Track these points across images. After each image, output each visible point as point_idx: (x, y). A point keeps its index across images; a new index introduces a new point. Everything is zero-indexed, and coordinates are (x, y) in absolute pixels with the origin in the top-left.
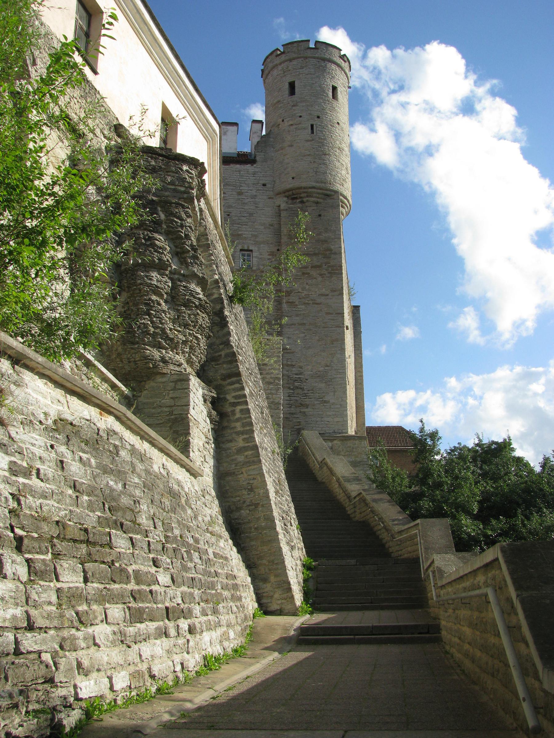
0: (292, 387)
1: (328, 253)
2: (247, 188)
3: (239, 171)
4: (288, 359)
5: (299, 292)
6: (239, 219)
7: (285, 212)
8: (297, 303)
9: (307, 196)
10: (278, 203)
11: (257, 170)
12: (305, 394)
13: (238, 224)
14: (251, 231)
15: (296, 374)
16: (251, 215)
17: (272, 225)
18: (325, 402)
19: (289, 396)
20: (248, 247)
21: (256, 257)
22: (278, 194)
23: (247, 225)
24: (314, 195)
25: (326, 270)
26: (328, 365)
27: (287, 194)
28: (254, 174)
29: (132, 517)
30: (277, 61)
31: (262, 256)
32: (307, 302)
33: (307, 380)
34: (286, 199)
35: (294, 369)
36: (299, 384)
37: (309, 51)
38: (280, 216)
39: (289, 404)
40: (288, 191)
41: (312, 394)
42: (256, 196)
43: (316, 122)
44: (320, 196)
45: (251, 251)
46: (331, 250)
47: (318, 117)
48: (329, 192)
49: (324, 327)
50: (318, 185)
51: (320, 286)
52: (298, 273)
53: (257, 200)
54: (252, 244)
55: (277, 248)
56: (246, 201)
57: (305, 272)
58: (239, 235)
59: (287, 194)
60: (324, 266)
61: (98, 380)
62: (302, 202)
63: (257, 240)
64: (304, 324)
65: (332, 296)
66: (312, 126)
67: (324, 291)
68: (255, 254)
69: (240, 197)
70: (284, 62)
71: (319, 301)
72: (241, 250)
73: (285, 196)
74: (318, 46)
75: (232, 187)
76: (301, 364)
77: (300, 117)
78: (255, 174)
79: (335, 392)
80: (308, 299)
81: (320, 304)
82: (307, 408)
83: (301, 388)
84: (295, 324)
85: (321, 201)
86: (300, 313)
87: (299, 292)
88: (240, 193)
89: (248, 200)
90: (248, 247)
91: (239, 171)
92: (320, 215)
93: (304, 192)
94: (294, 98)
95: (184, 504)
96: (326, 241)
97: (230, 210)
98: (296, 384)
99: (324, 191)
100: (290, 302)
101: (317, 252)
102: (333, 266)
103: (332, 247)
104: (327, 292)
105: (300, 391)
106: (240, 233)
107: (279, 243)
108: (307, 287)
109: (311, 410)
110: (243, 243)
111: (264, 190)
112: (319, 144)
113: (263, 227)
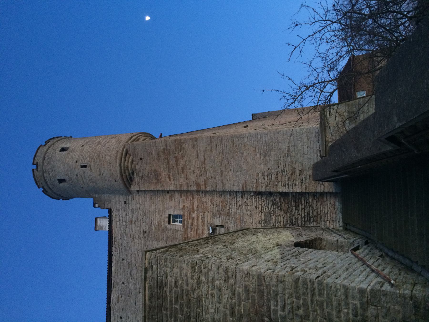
0: (276, 183)
1: (166, 152)
4: (251, 187)
5: (197, 176)
7: (141, 187)
9: (128, 170)
11: (115, 209)
12: (282, 170)
13: (151, 225)
15: (264, 179)
17: (151, 198)
18: (288, 151)
19: (285, 186)
20: (167, 217)
21: (174, 212)
24: (126, 163)
25: (178, 153)
26: (254, 149)
27: (128, 185)
28: (118, 210)
29: (334, 122)
31: (173, 206)
32: (203, 169)
33: (269, 169)
35: (260, 181)
36: (273, 176)
40: (125, 184)
41: (282, 163)
43: (80, 164)
44: (127, 159)
45: (170, 215)
46: (164, 149)
47: (77, 162)
48: (124, 153)
49: (223, 154)
51: (191, 158)
52: (183, 176)
54: (164, 214)
55: (166, 193)
56: (135, 217)
57: (181, 171)
58: (159, 225)
59: (128, 185)
60: (176, 155)
62: (133, 173)
64: (221, 171)
65: (197, 147)
66: (82, 167)
67: (194, 155)
68: (172, 213)
69: (133, 222)
71: (202, 159)
72: (169, 223)
73: (130, 187)
74: (35, 163)
76: (255, 174)
77: (77, 175)
79: (279, 142)
82: (295, 168)
83: (277, 174)
84: (222, 180)
86: (213, 176)
87: (197, 176)
88: (131, 222)
90: (167, 217)
92: (141, 159)
93: (125, 172)
96: (158, 154)
98: (273, 178)
100: (205, 184)
101: (166, 161)
102: (176, 148)
103: (162, 148)
104: (195, 152)
105: (280, 175)
107: (163, 191)
108: (192, 169)
109: (297, 164)
110: (164, 221)
112: (93, 161)
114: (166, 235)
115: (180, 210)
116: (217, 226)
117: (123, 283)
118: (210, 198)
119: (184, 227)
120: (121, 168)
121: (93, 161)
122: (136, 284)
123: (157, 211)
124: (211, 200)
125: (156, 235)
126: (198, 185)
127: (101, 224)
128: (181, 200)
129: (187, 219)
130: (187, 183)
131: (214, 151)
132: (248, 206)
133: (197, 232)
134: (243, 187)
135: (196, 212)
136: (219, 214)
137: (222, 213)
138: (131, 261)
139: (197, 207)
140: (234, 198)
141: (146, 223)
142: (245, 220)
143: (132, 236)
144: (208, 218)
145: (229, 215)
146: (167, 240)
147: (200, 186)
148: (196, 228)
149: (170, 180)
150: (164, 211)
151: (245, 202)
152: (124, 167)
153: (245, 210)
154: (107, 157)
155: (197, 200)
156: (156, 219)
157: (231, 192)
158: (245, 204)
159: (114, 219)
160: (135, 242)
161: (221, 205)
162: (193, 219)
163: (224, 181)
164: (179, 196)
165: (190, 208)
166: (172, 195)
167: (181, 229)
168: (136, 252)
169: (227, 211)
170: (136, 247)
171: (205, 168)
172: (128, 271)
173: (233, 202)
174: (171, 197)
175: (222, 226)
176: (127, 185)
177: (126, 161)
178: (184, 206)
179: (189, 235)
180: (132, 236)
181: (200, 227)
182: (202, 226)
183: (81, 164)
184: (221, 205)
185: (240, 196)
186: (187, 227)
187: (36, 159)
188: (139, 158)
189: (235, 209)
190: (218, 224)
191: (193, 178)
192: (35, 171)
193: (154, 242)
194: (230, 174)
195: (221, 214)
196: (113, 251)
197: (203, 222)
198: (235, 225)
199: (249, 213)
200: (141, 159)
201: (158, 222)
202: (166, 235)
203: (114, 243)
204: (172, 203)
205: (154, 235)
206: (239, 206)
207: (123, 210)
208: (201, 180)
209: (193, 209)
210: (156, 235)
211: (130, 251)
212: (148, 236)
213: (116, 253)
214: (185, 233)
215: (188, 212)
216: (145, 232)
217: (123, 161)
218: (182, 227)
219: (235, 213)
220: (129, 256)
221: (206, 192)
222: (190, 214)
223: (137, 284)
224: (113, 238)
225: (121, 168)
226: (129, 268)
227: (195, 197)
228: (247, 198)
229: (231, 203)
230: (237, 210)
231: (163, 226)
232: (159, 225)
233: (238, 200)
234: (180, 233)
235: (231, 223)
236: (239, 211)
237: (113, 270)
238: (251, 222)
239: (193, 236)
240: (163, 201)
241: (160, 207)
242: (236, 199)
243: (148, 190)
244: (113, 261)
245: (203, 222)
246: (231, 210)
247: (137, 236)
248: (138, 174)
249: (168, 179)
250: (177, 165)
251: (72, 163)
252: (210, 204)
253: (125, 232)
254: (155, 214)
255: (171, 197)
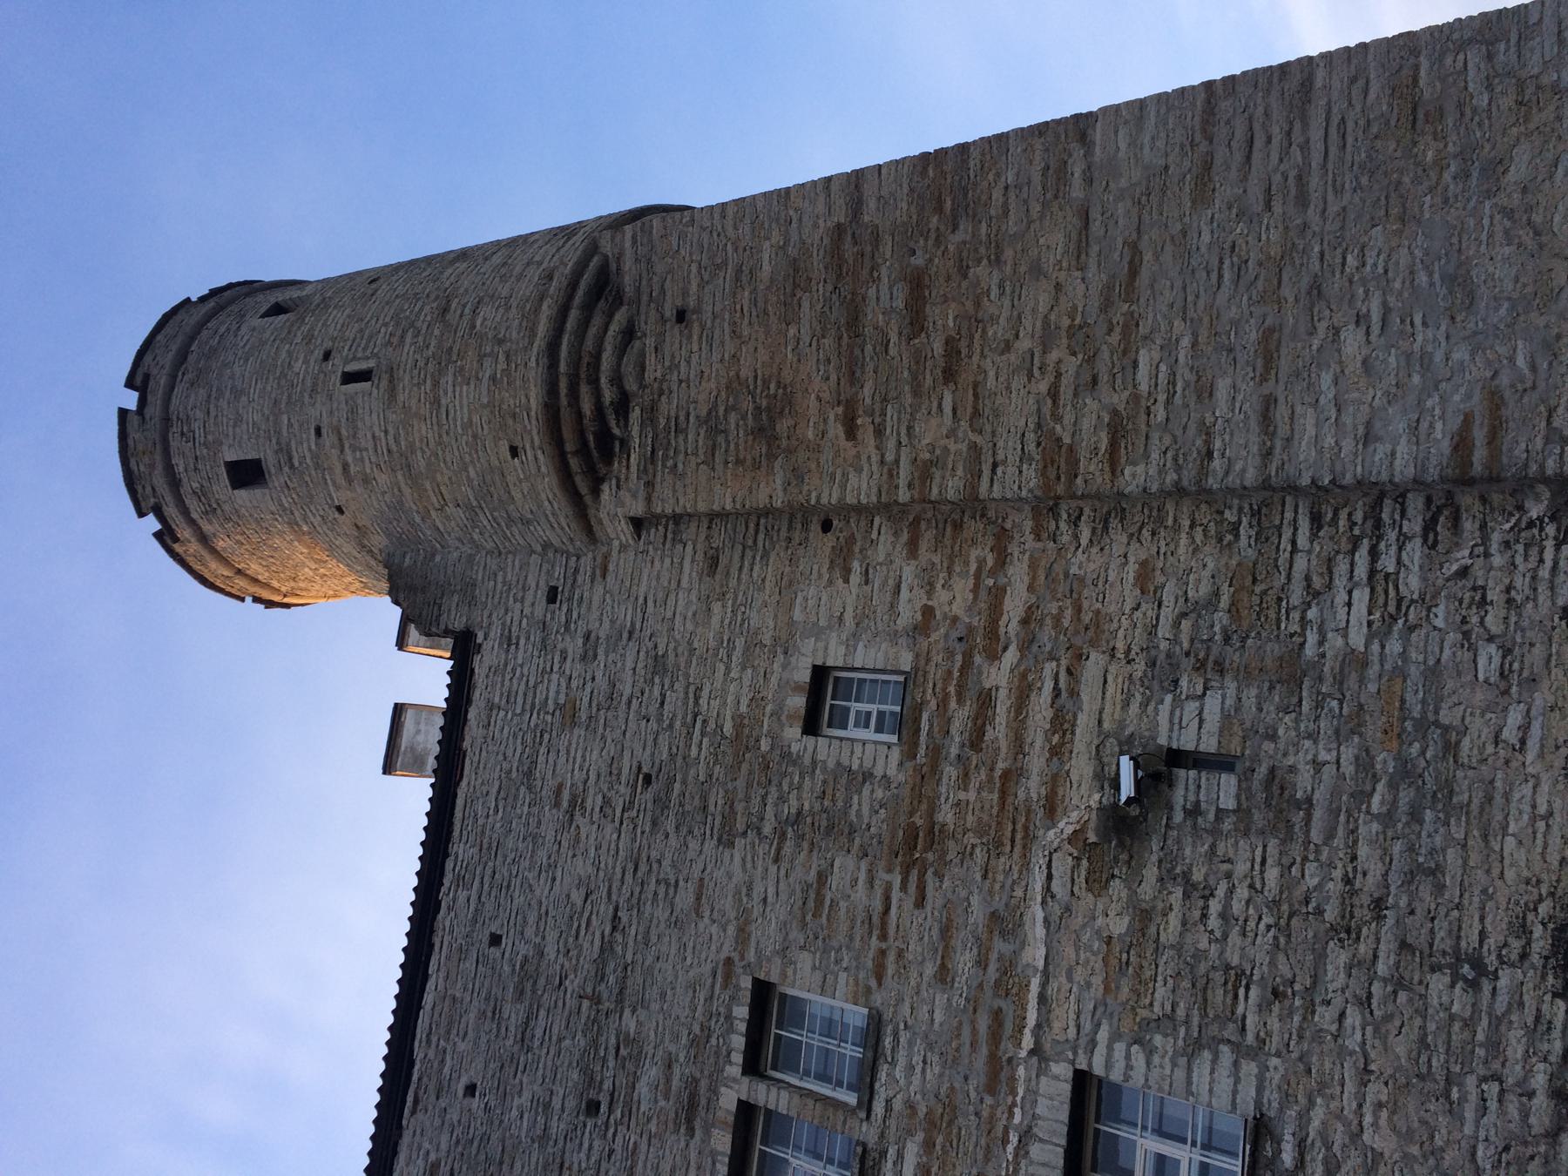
2: (555, 677)
3: (491, 707)
5: (1054, 393)
6: (671, 726)
8: (1119, 400)
9: (594, 382)
10: (624, 531)
11: (495, 632)
13: (690, 735)
14: (728, 669)
16: (658, 664)
20: (797, 688)
21: (850, 648)
22: (589, 531)
23: (699, 689)
24: (589, 344)
28: (509, 641)
30: (184, 532)
32: (1115, 338)
34: (605, 487)
37: (148, 411)
38: (677, 519)
39: (814, 762)
42: (587, 637)
50: (543, 328)
53: (602, 635)
54: (784, 667)
55: (815, 527)
56: (602, 683)
59: (584, 489)
61: (1267, 1093)
62: (623, 405)
63: (767, 640)
70: (185, 512)
72: (811, 726)
73: (596, 492)
75: (543, 750)
78: (510, 639)
80: (1100, 330)
81: (1134, 248)
84: (1269, 402)
85: (620, 317)
87: (1054, 393)
89: (599, 675)
90: (797, 688)
91: (491, 707)
94: (270, 461)
95: (1013, 648)
97: (625, 771)
99: (577, 300)
106: (728, 728)
111: (570, 599)
113: (717, 607)
114: (782, 799)
115: (894, 637)
116: (1176, 758)
117: (471, 1090)
118: (1137, 553)
119: (910, 753)
120: (553, 365)
121: (408, 340)
122: (547, 1106)
123: (740, 643)
124: (1144, 564)
125: (717, 799)
126: (1057, 457)
127: (420, 738)
128: (909, 572)
129: (943, 704)
130: (974, 447)
131: (1225, 191)
132: (1483, 602)
133: (1003, 794)
134: (1462, 444)
135: (1011, 656)
136: (1200, 667)
137: (1234, 657)
138: (541, 954)
139: (1025, 622)
140: (1355, 543)
141: (660, 720)
142: (1445, 717)
143: (566, 795)
144: (1102, 694)
145: (1291, 674)
146: (783, 835)
147: (1074, 462)
148: (1001, 765)
149: (851, 433)
150: (785, 646)
151: (1464, 572)
152: (575, 363)
153: (1453, 637)
154: (486, 311)
155: (1033, 566)
156: (728, 695)
157: (1321, 500)
158: (1457, 588)
159: (476, 695)
160: (577, 840)
161: (1225, 601)
162: (986, 700)
163: (1281, 413)
164: (900, 552)
165: (971, 629)
166: (851, 540)
167: (892, 770)
168: (577, 897)
169: (1273, 649)
170: (582, 867)
171: (1132, 322)
172: (513, 1014)
173: (1340, 583)
174: (841, 561)
175: (1219, 763)
176: (578, 479)
177: (593, 331)
178: (928, 612)
179: (946, 815)
180: (566, 795)
181: (1036, 763)
182: (1055, 752)
183: (347, 362)
184: (1225, 601)
185: (1414, 526)
186: (936, 753)
187: (148, 358)
188: (669, 312)
189: (1357, 639)
190: (1187, 742)
191: (1017, 408)
192: (134, 421)
193: (693, 845)
194: (1352, 341)
195: (1220, 669)
196: (446, 882)
197: (1062, 723)
198: (1348, 754)
199: (1488, 659)
200: (681, 316)
201: (739, 726)
202: (782, 799)
203: (456, 833)
204: (850, 593)
205: (704, 799)
206: (1391, 612)
207: (536, 637)
208: (1086, 425)
209: (992, 632)
210: (717, 799)
211: (542, 889)
212: (661, 803)
213: (462, 895)
214: (917, 794)
215: (950, 654)
216: (648, 779)
217: (570, 324)
218: (896, 754)
219: (1356, 661)
220: (532, 919)
221: (1113, 510)
222: (967, 664)
223: (556, 1103)
224: (460, 802)
225: (553, 365)
226: (520, 994)
227: (1014, 549)
228: (1485, 540)
229: (1317, 582)
230: (1378, 633)
231: (765, 745)
232: (743, 740)
233: (1388, 563)
234: (879, 794)
235: (1313, 736)
236: (1394, 646)
237: (429, 999)
238: (1510, 734)
239: (970, 820)
240: (787, 587)
241: (764, 621)
242: (1374, 554)
243: (702, 507)
244: (437, 941)
245: (1062, 723)
246: (1312, 638)
247: (593, 801)
248: (651, 412)
249: (836, 430)
250: (916, 322)
251: (306, 362)
252: (1131, 595)
253: (529, 774)
254: (721, 667)
255: (841, 561)
